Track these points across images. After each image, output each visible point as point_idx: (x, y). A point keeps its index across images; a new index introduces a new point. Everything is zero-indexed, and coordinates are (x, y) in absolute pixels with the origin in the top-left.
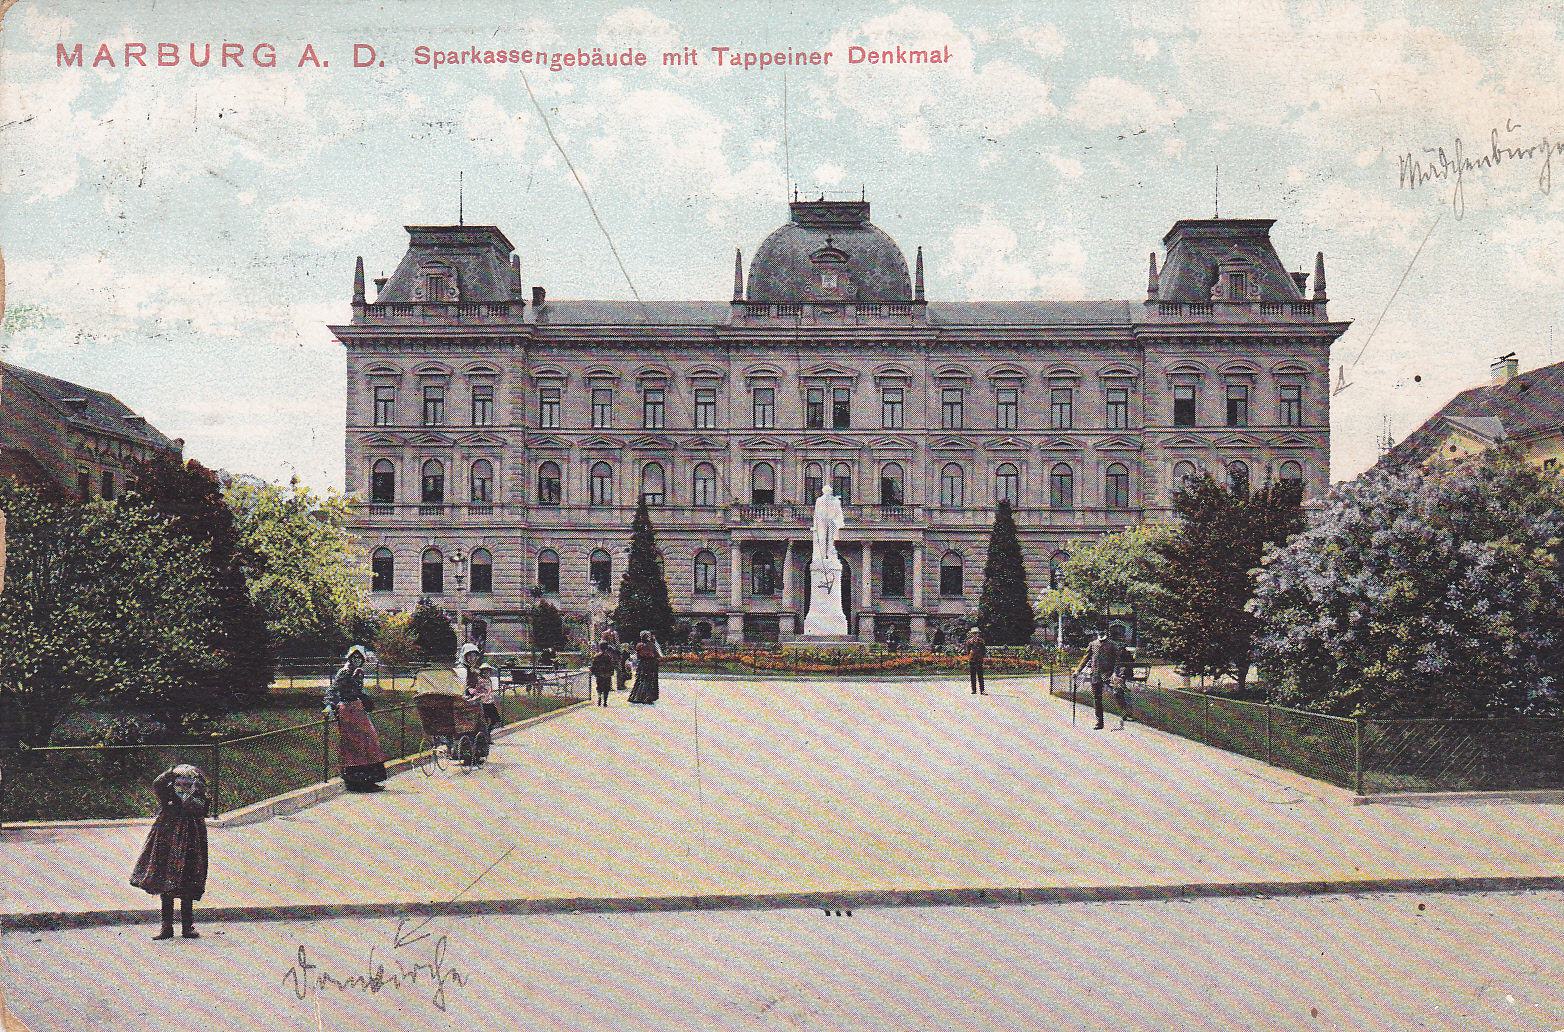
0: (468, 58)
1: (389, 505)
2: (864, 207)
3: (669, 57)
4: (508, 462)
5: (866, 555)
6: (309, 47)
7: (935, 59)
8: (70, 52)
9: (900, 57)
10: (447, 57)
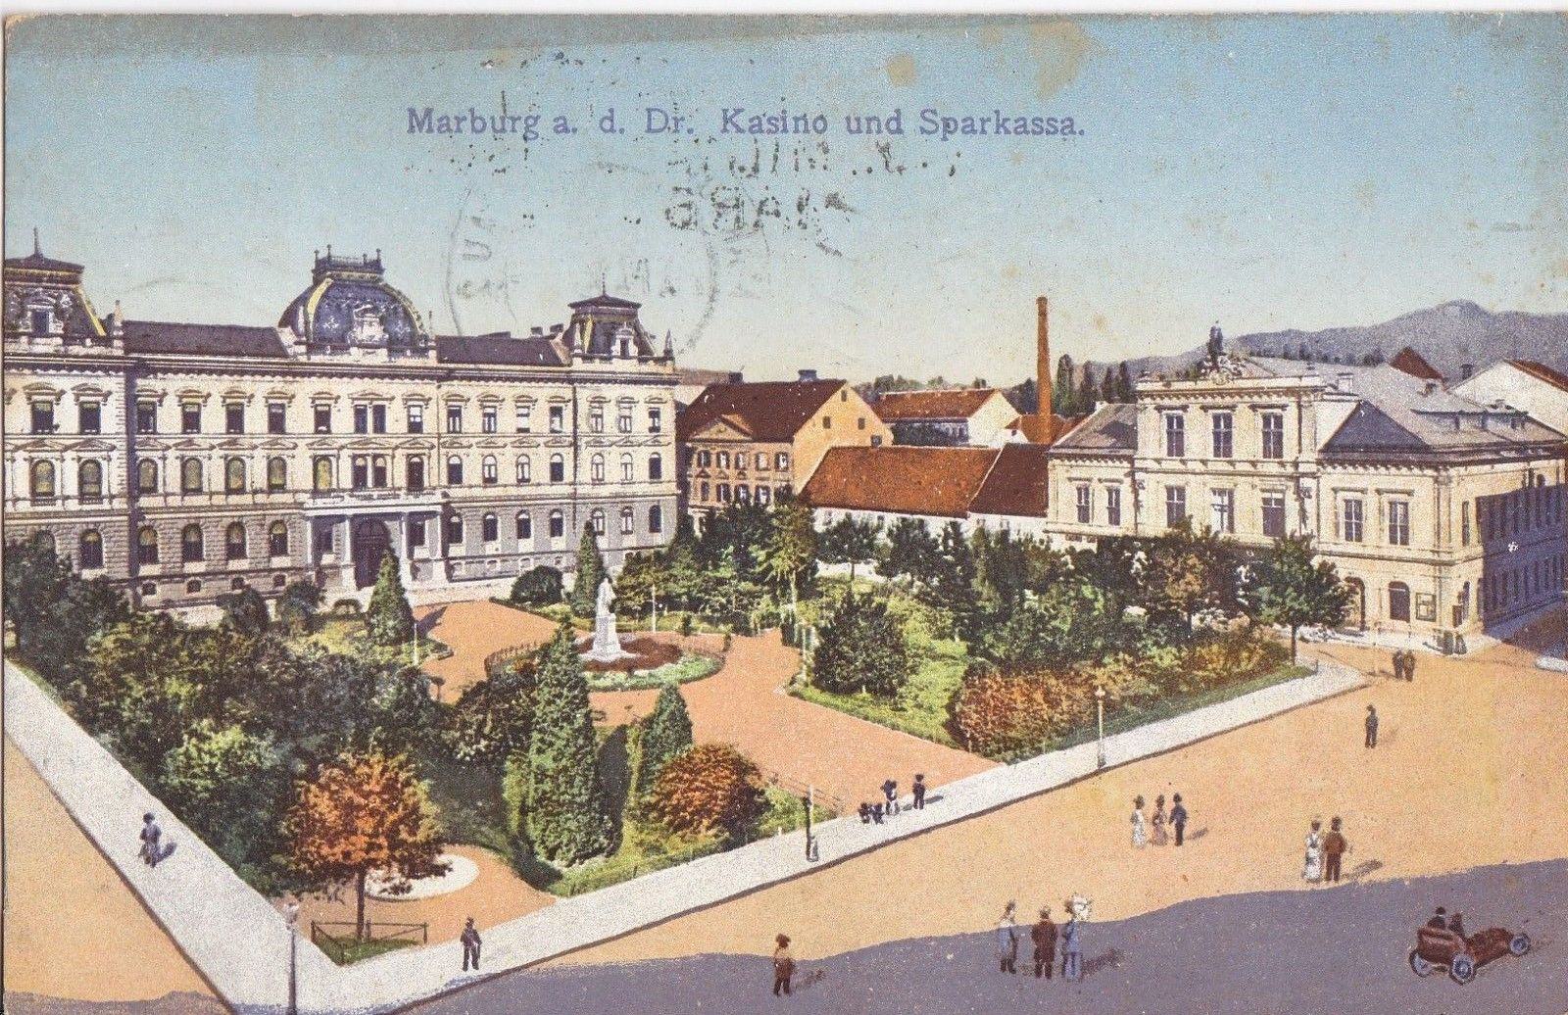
0: (466, 125)
1: (653, 405)
2: (77, 269)
3: (1022, 123)
4: (115, 463)
5: (347, 523)
6: (538, 117)
7: (444, 129)
8: (420, 114)
9: (1001, 126)
10: (961, 125)
